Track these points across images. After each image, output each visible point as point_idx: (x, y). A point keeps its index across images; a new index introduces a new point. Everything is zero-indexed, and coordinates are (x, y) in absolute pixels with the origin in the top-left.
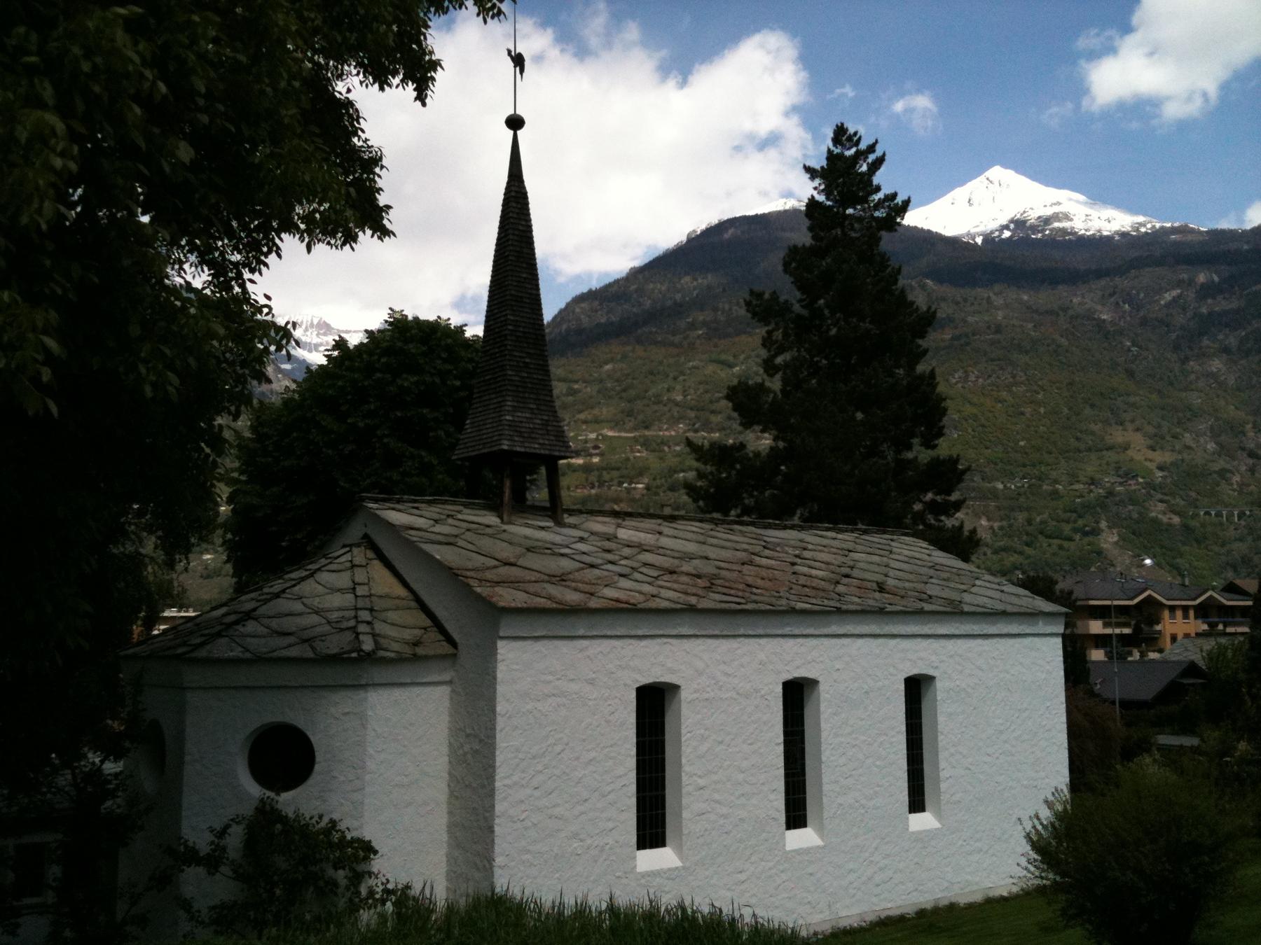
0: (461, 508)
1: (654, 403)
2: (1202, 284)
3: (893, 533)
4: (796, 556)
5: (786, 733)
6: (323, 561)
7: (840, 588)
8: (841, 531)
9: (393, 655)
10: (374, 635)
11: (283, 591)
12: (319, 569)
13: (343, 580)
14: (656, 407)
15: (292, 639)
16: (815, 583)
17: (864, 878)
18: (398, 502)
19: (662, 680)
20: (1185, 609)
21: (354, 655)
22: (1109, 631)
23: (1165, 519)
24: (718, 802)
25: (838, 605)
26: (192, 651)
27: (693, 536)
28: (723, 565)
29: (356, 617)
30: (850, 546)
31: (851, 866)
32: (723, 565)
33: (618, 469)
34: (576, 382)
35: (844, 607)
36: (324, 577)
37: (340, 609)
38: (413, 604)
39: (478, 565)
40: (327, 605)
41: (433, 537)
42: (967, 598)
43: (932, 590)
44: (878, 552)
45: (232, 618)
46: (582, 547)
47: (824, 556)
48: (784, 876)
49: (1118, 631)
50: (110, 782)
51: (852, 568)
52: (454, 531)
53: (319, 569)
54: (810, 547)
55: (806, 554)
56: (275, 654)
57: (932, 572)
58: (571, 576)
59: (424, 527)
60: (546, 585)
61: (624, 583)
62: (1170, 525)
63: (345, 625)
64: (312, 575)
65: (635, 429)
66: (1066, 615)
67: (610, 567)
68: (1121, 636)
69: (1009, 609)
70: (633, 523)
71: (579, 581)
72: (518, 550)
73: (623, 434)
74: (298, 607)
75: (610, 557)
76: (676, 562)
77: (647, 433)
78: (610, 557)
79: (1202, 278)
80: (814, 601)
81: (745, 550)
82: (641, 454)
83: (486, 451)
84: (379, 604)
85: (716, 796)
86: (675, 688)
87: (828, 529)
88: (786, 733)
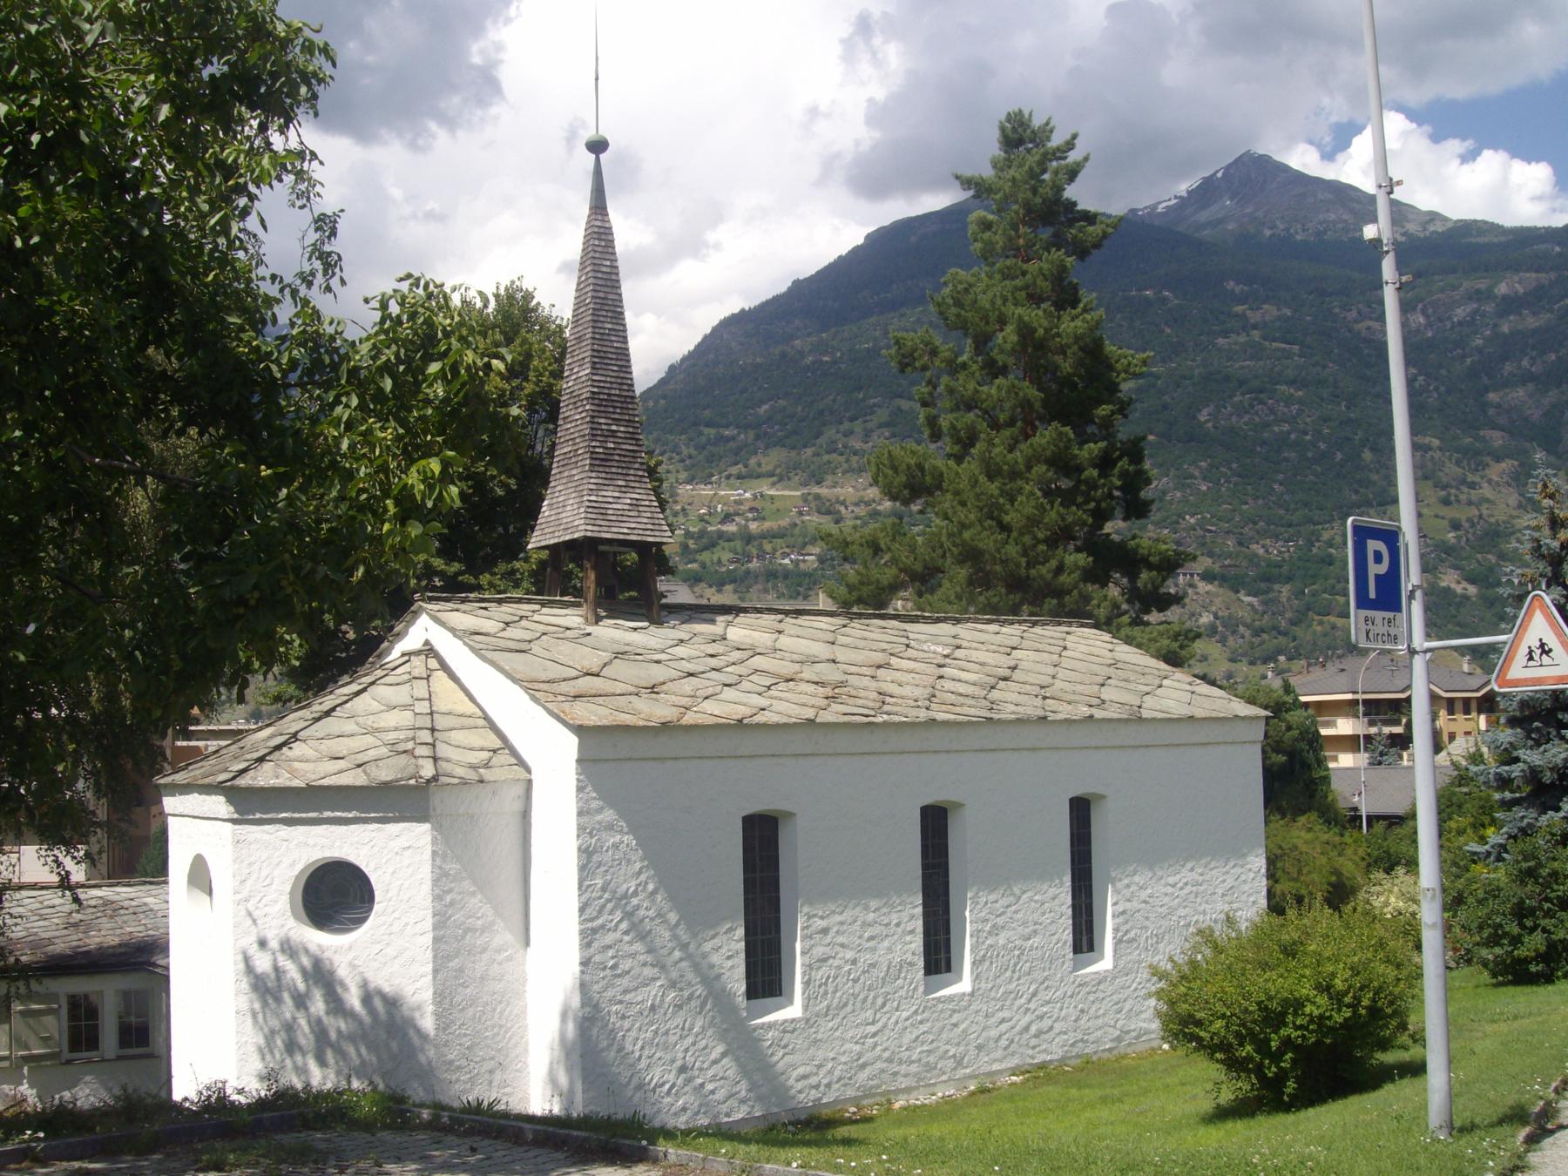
0: (537, 607)
1: (828, 452)
2: (1504, 297)
3: (1070, 624)
4: (946, 656)
5: (925, 867)
6: (379, 673)
7: (995, 694)
8: (1003, 623)
9: (456, 781)
10: (435, 759)
11: (333, 709)
12: (373, 683)
13: (401, 695)
14: (826, 457)
15: (341, 764)
16: (962, 688)
17: (1018, 1028)
18: (463, 601)
19: (772, 807)
20: (1467, 701)
21: (412, 782)
22: (1373, 730)
23: (1459, 589)
24: (842, 945)
25: (988, 715)
26: (234, 778)
27: (820, 634)
28: (853, 669)
29: (414, 739)
30: (1015, 641)
31: (1005, 1014)
32: (853, 669)
33: (782, 536)
34: (727, 426)
35: (996, 716)
36: (380, 690)
37: (396, 729)
38: (482, 722)
39: (551, 676)
40: (382, 724)
41: (503, 644)
42: (1149, 702)
43: (1107, 694)
44: (1048, 648)
45: (280, 740)
46: (680, 651)
47: (981, 656)
48: (923, 1028)
49: (1387, 730)
50: (1224, 628)
51: (1014, 668)
52: (528, 636)
53: (373, 683)
54: (965, 644)
55: (958, 653)
56: (325, 782)
57: (1111, 671)
58: (664, 687)
59: (492, 631)
60: (632, 698)
61: (729, 693)
62: (1466, 598)
63: (401, 747)
64: (364, 690)
65: (805, 484)
66: (1267, 718)
67: (714, 675)
68: (1392, 736)
69: (1199, 713)
70: (748, 621)
71: (674, 693)
72: (606, 656)
73: (786, 493)
74: (350, 727)
75: (714, 662)
76: (797, 667)
77: (816, 490)
78: (714, 662)
79: (1502, 289)
80: (958, 710)
81: (884, 651)
82: (813, 520)
83: (567, 538)
84: (440, 722)
85: (841, 939)
86: (790, 815)
87: (989, 622)
88: (925, 867)
